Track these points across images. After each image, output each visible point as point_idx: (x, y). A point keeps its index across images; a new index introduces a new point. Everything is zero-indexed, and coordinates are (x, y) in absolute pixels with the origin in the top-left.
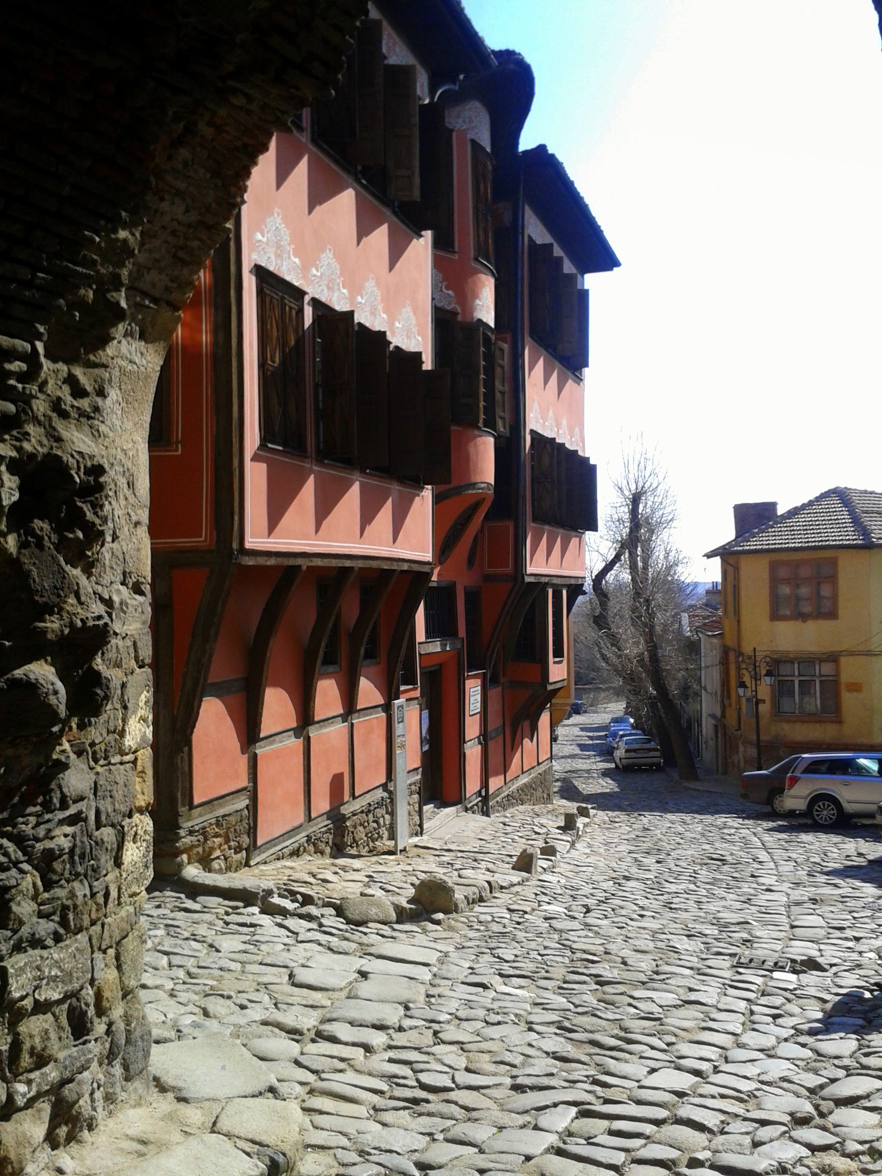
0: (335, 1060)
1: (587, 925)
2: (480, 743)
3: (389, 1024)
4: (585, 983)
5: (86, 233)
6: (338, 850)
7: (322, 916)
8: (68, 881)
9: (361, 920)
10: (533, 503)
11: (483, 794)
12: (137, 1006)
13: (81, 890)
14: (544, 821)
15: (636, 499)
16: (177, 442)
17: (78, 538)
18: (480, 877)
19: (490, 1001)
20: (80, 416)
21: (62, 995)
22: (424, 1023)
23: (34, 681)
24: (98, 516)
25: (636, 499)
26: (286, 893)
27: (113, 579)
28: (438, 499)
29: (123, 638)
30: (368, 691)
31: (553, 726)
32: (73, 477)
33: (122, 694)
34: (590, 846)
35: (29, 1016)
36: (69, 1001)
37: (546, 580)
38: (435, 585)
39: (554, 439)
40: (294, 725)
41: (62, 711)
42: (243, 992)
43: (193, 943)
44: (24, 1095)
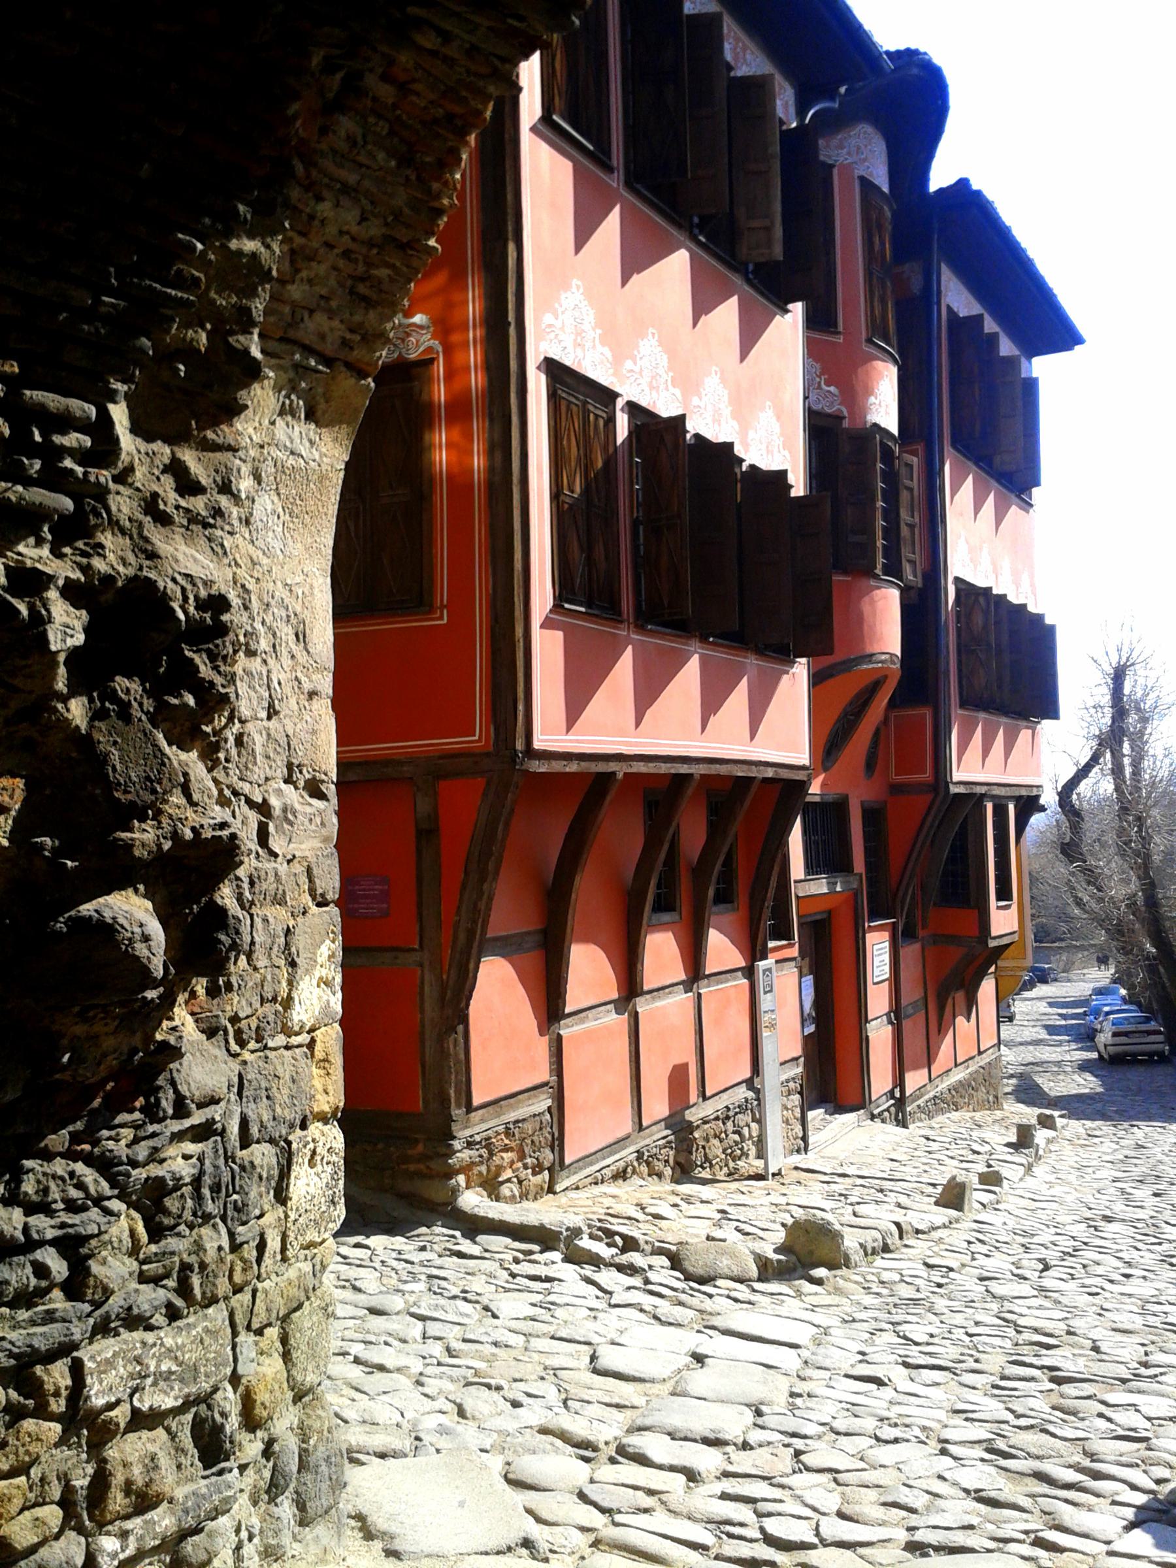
0: (640, 1493)
1: (1042, 1289)
2: (890, 1022)
3: (727, 1437)
4: (1032, 1379)
5: (180, 236)
6: (684, 1172)
7: (650, 1267)
8: (191, 1227)
9: (706, 1275)
10: (960, 682)
11: (898, 1095)
12: (320, 1412)
13: (214, 1239)
14: (987, 1134)
15: (1119, 676)
16: (442, 607)
17: (186, 705)
18: (883, 1216)
19: (886, 1405)
20: (189, 521)
21: (180, 1401)
22: (782, 1437)
23: (110, 921)
24: (219, 673)
25: (1119, 676)
26: (600, 1233)
27: (269, 773)
28: (816, 679)
29: (289, 862)
30: (721, 949)
31: (1002, 1000)
32: (174, 611)
33: (287, 944)
34: (1055, 1170)
35: (124, 1434)
36: (194, 1410)
37: (983, 790)
38: (817, 799)
39: (991, 588)
40: (615, 996)
41: (157, 967)
42: (521, 1380)
43: (460, 1303)
44: (114, 1555)
